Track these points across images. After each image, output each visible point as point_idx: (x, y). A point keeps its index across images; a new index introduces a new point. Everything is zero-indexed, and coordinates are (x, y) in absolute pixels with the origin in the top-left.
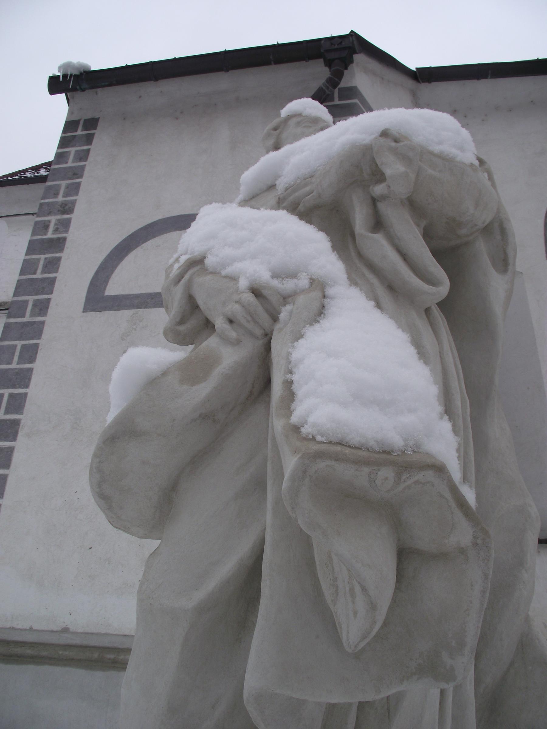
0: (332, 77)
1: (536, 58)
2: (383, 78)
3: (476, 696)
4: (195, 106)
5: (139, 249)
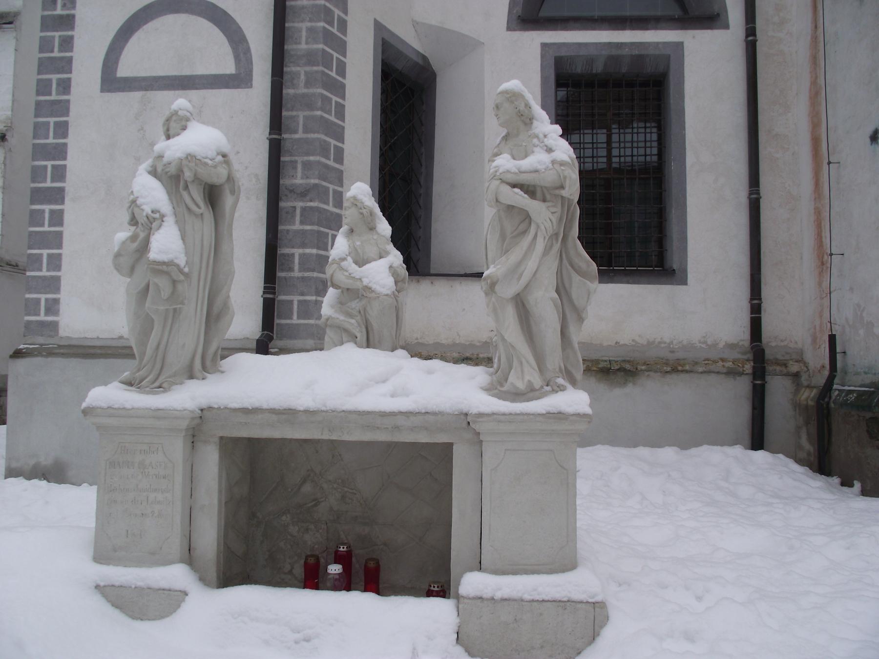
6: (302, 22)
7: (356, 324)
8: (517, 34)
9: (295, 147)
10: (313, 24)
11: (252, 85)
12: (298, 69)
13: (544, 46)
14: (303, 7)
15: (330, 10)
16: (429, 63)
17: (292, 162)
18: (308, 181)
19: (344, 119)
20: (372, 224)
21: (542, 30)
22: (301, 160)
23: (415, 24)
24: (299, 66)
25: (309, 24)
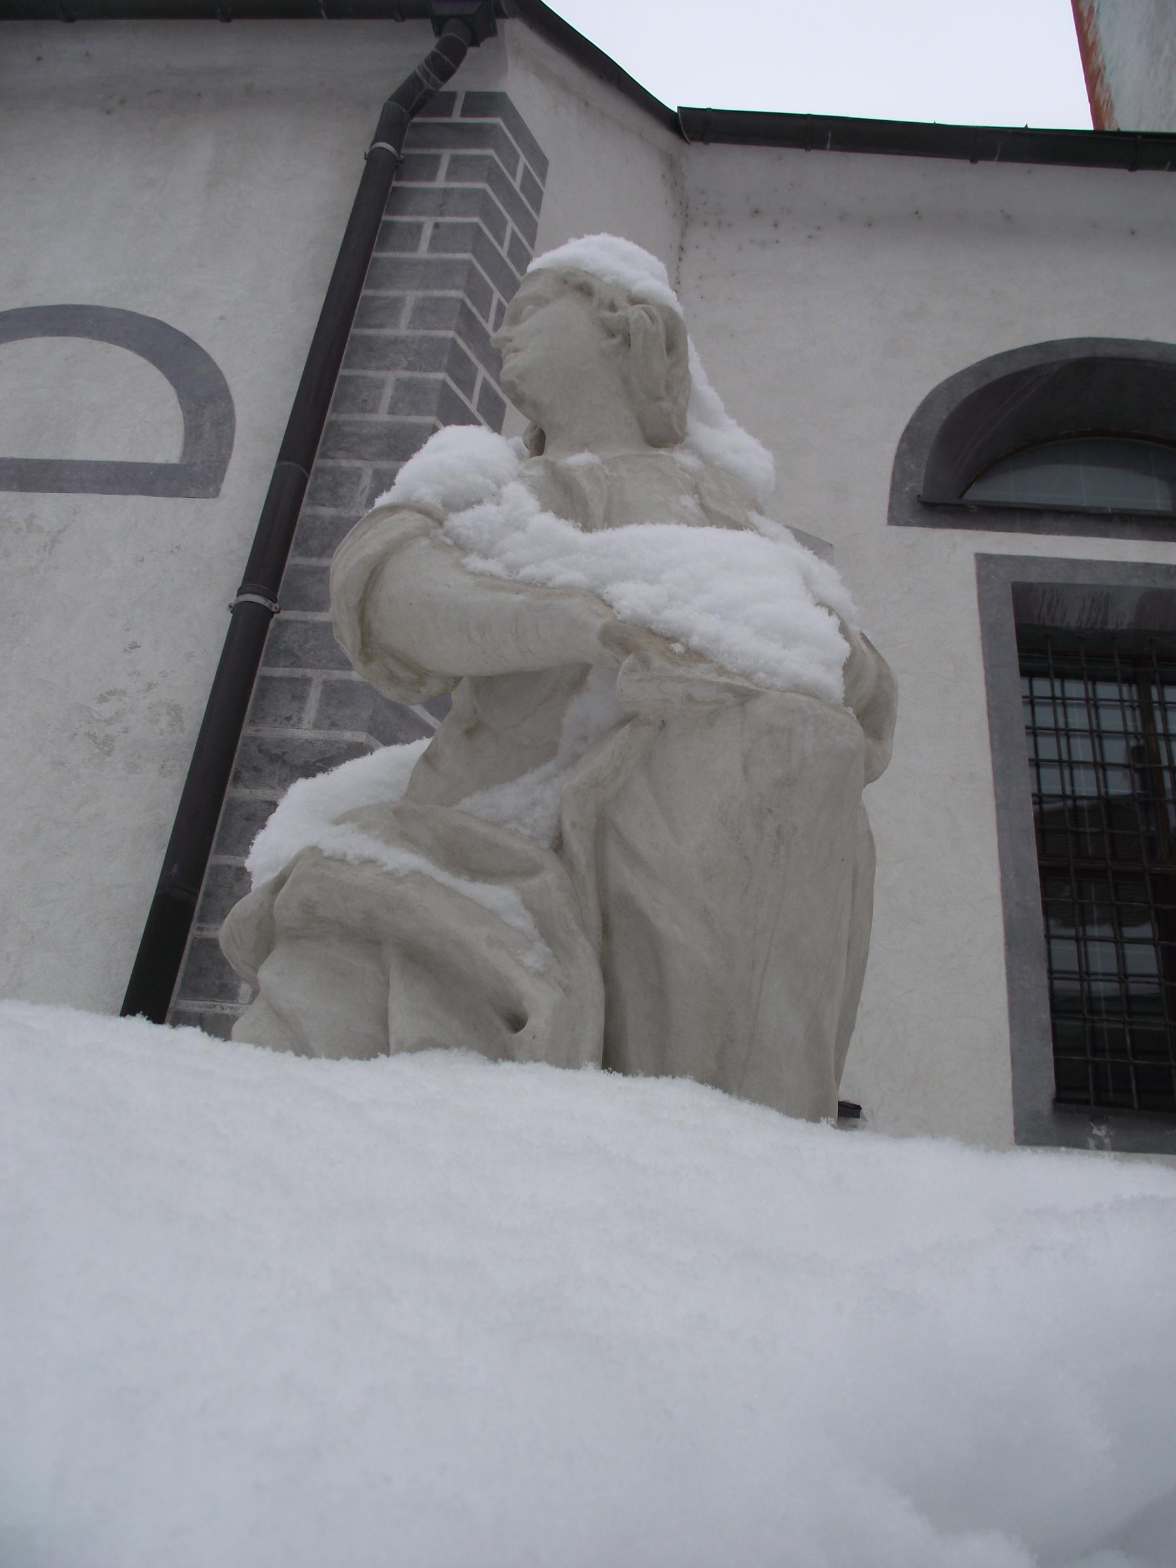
0: (438, 52)
1: (933, 122)
2: (587, 104)
3: (228, 963)
4: (155, 91)
5: (185, 780)
6: (388, 369)
7: (523, 922)
8: (915, 534)
9: (309, 645)
10: (418, 375)
12: (358, 463)
13: (983, 560)
14: (396, 341)
15: (465, 357)
17: (292, 680)
18: (335, 734)
20: (666, 405)
21: (977, 528)
22: (324, 677)
24: (360, 457)
25: (406, 375)
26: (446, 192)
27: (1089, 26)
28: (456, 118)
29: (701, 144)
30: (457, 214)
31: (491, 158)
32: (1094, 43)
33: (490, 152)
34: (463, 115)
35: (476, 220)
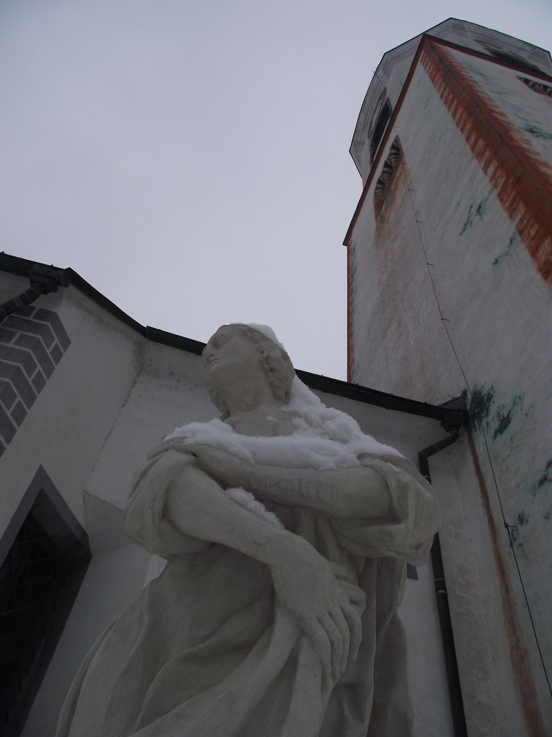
0: (26, 294)
2: (101, 320)
11: (2, 252)
16: (87, 541)
19: (32, 405)
23: (86, 495)
26: (12, 349)
27: (351, 316)
28: (31, 318)
29: (153, 342)
30: (12, 360)
31: (39, 339)
32: (351, 323)
33: (39, 337)
34: (34, 318)
35: (19, 365)
